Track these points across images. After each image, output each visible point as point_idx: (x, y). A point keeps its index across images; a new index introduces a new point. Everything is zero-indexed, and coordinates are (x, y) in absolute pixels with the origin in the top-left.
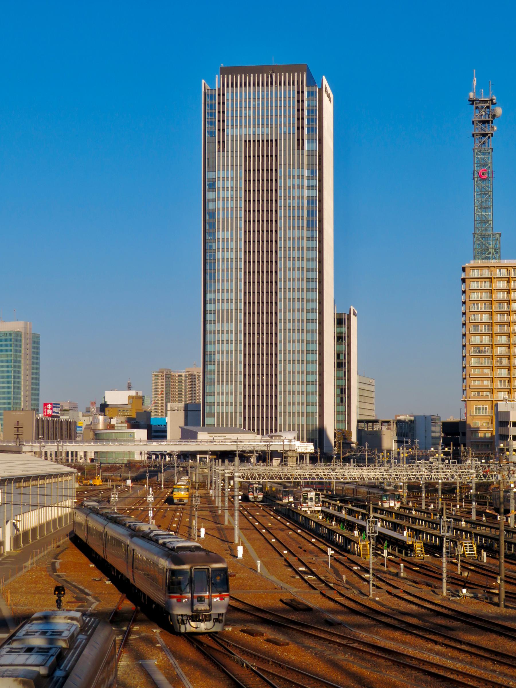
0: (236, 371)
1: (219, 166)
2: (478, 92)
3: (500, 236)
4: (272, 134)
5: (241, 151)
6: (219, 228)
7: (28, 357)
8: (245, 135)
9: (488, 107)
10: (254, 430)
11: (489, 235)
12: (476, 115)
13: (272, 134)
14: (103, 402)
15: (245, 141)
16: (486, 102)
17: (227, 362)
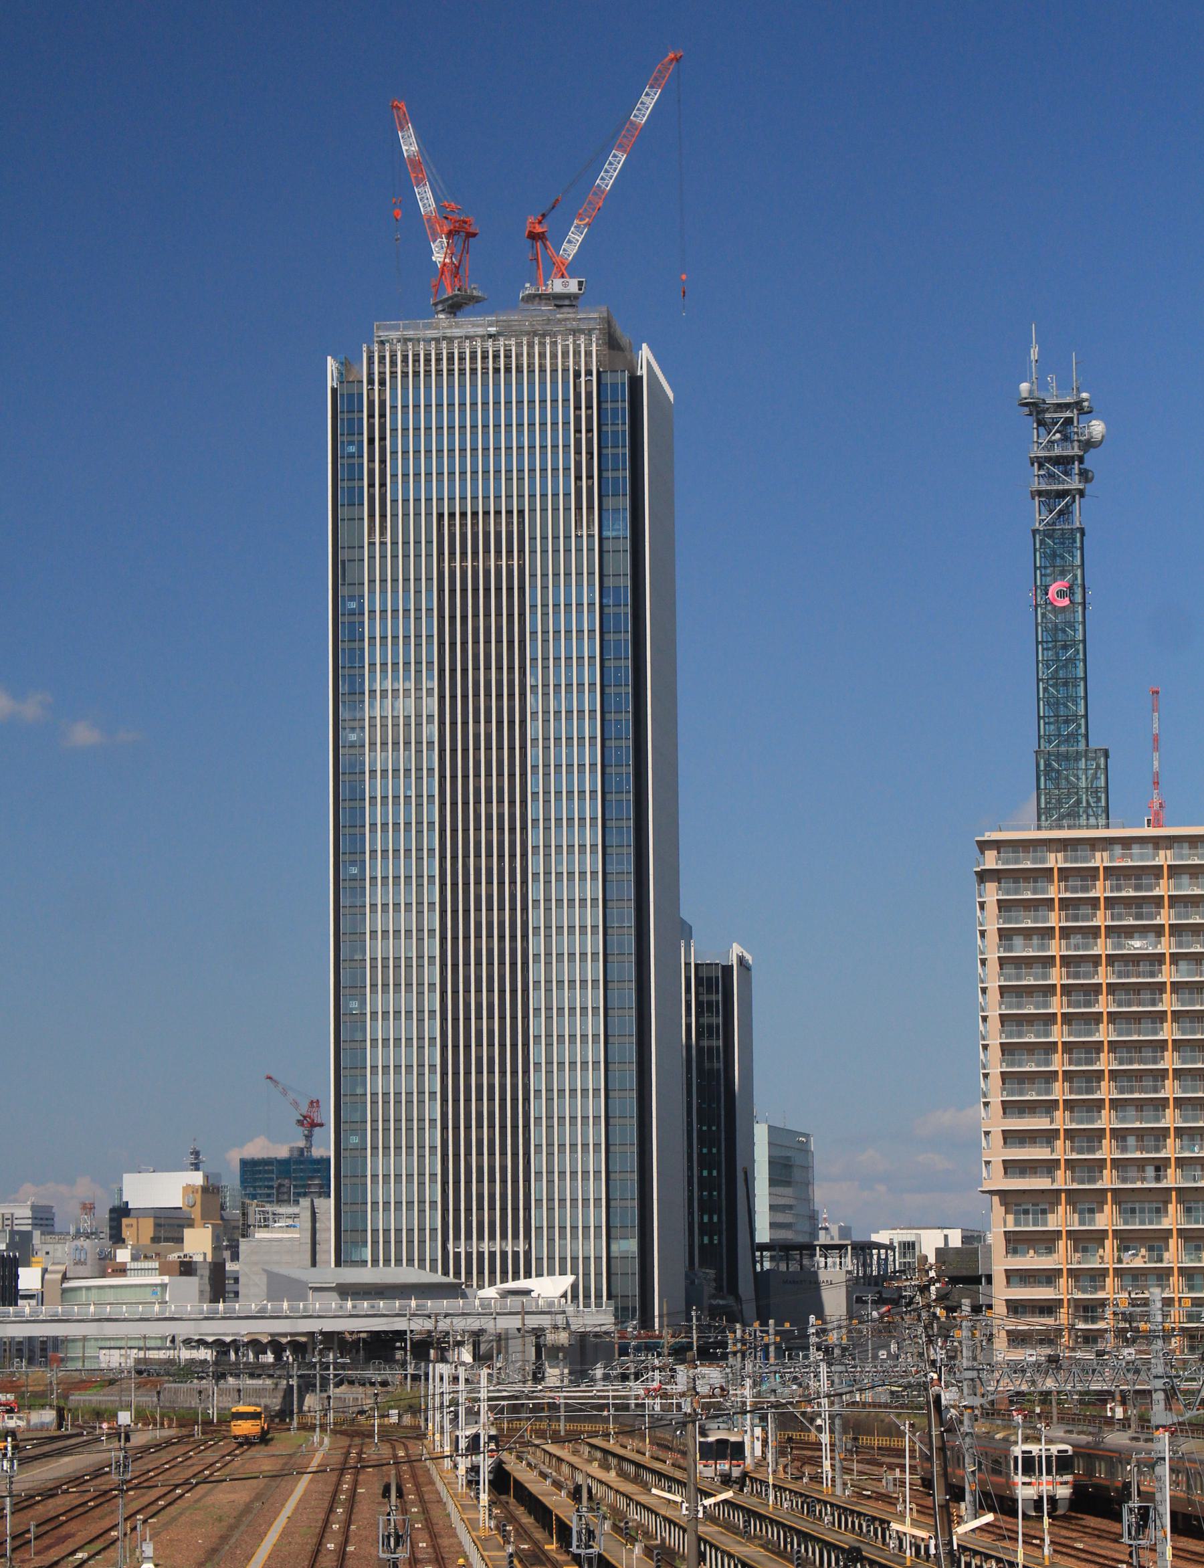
0: (421, 1120)
1: (372, 581)
2: (1042, 385)
3: (1107, 757)
4: (509, 497)
5: (429, 542)
6: (374, 986)
7: (1143, 1455)
8: (440, 499)
9: (1069, 421)
10: (422, 1260)
11: (1077, 756)
12: (1039, 443)
13: (509, 497)
14: (117, 1203)
15: (440, 516)
16: (1067, 406)
17: (398, 1094)
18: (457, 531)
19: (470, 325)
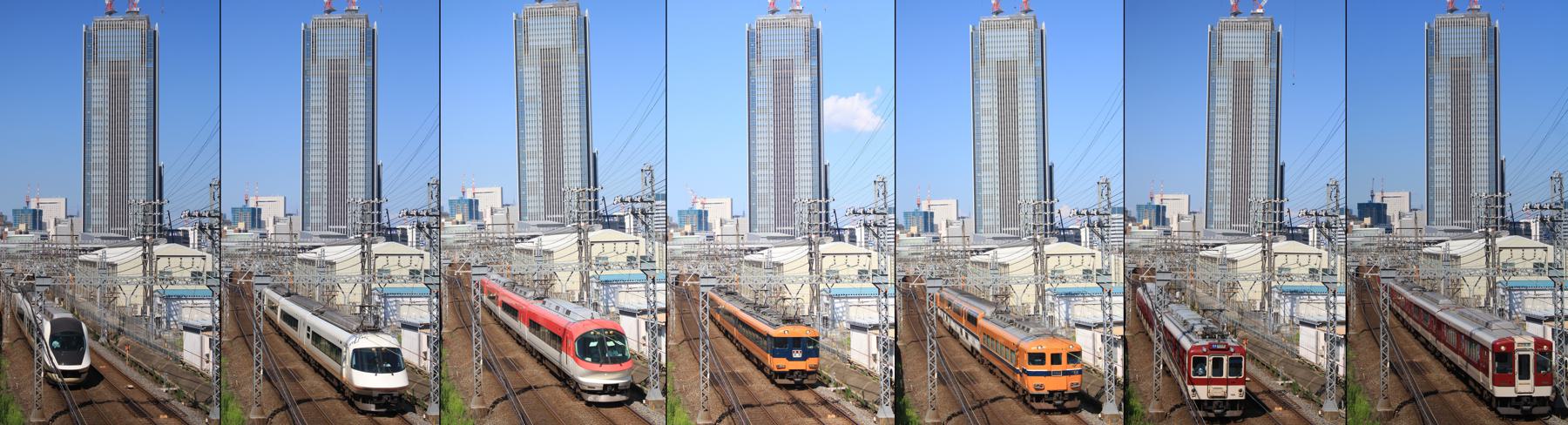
18: (332, 64)
19: (333, 16)
